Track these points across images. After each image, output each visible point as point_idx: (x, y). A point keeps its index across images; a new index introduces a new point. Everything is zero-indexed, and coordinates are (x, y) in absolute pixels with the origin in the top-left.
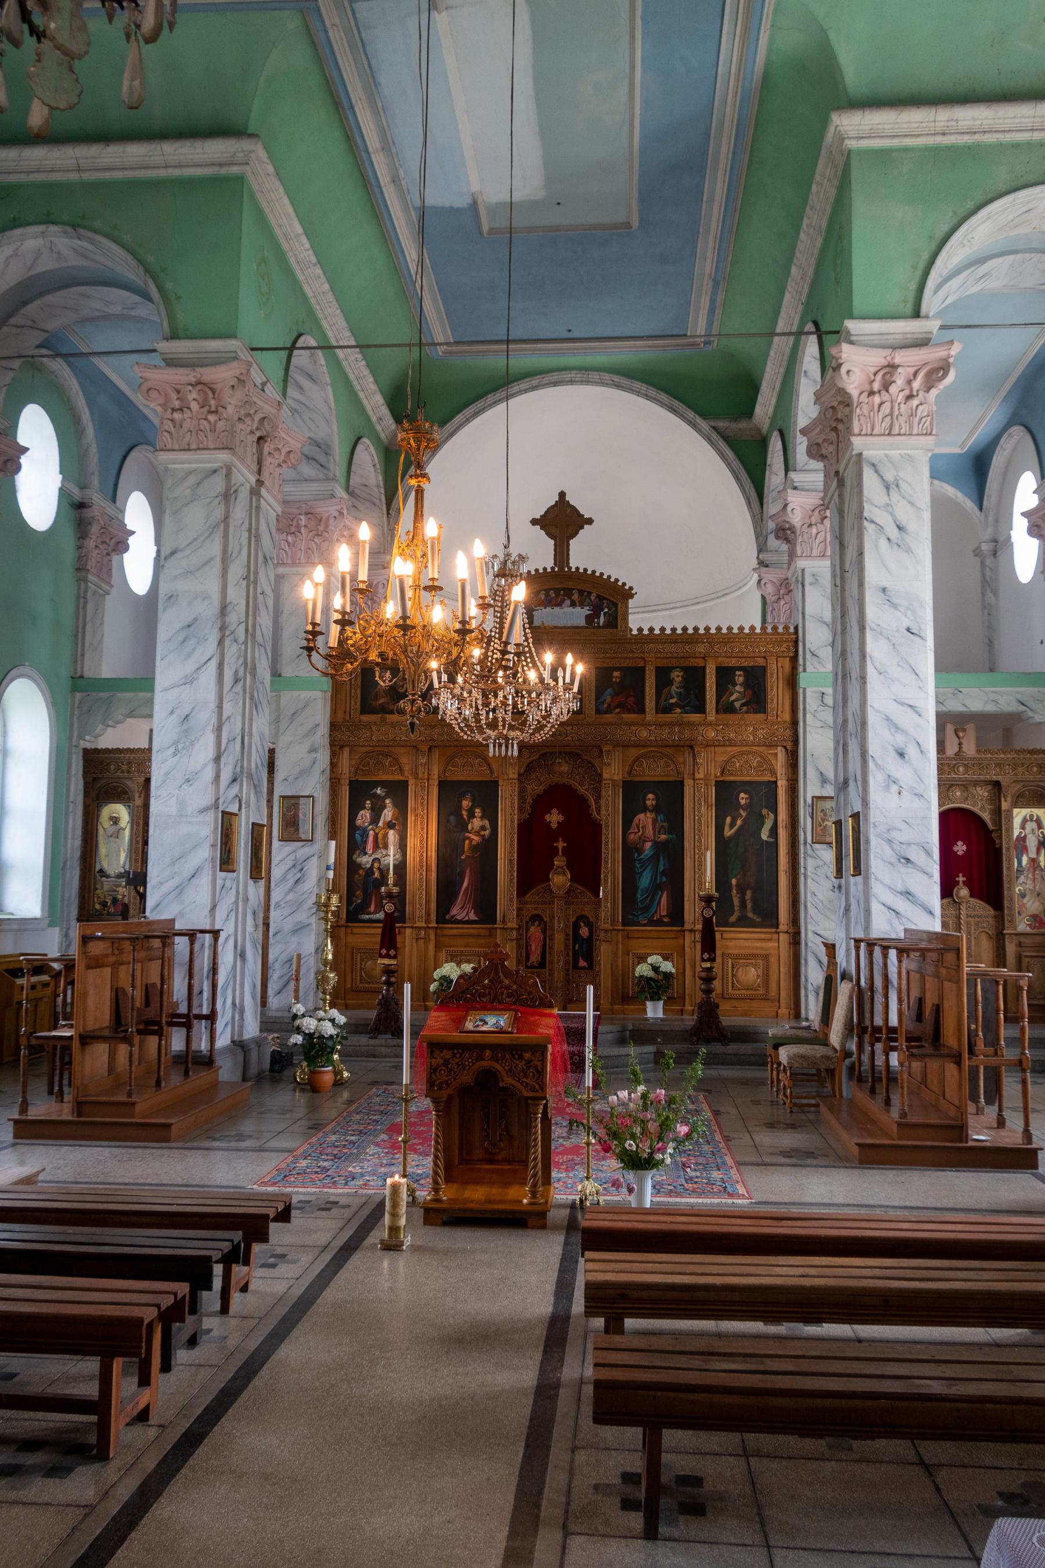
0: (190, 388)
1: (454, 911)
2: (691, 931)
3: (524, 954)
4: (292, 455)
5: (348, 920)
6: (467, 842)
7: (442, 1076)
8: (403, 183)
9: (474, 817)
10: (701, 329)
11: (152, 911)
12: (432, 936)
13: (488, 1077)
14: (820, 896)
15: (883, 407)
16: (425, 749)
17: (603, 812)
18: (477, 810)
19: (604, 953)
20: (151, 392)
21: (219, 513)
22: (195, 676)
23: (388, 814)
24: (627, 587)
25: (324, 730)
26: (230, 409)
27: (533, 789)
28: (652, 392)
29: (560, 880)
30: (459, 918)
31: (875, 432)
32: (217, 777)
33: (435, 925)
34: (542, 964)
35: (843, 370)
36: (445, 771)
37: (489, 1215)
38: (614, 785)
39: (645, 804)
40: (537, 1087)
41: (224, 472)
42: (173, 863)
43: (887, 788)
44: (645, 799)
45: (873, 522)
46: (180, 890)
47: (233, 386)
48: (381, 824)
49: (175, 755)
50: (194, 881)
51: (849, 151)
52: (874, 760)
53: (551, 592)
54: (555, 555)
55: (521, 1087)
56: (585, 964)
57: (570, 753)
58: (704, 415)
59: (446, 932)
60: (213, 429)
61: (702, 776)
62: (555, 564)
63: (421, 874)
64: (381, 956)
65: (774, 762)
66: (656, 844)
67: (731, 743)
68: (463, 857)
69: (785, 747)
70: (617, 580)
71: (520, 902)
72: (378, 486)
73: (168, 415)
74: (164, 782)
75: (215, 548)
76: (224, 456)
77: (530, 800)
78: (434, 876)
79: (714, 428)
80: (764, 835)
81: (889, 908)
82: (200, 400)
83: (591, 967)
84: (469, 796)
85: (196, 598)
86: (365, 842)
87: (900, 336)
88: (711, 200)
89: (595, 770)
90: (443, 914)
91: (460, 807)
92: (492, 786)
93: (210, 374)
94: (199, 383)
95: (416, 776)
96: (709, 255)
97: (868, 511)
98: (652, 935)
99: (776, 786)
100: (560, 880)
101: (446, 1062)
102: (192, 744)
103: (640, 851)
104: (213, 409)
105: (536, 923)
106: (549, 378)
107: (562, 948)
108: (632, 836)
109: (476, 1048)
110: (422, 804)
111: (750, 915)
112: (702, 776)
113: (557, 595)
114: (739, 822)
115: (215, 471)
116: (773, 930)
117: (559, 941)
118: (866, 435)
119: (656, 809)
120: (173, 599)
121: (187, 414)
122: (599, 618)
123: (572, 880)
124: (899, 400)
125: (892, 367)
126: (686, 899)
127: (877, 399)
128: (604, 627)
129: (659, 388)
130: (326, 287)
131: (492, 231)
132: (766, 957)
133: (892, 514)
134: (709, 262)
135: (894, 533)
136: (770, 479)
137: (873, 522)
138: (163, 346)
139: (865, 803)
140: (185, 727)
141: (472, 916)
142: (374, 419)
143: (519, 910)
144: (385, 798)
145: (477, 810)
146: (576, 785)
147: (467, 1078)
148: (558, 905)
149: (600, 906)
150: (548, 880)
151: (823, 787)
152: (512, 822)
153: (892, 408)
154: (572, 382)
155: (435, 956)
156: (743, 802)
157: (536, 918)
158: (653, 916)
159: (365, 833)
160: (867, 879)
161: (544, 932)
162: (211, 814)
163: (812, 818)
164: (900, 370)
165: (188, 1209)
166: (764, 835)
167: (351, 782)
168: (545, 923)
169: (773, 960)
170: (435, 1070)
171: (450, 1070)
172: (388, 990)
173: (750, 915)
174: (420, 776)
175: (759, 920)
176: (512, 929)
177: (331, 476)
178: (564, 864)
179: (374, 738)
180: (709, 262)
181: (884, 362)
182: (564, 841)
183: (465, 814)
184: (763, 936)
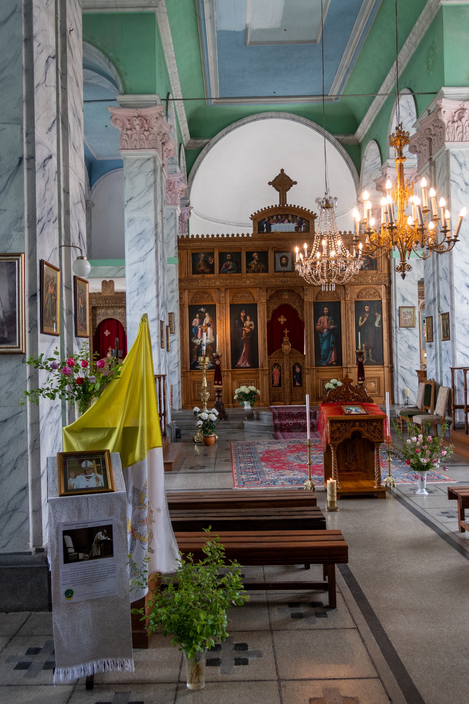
0: (135, 118)
1: (239, 363)
2: (346, 368)
3: (271, 381)
4: (171, 152)
5: (191, 369)
6: (244, 332)
7: (337, 435)
8: (215, 18)
9: (247, 320)
10: (335, 93)
12: (230, 375)
13: (357, 435)
14: (403, 350)
15: (459, 128)
16: (223, 290)
17: (305, 316)
18: (248, 317)
19: (307, 379)
20: (117, 120)
21: (152, 180)
22: (145, 257)
23: (207, 320)
24: (313, 214)
25: (176, 282)
26: (155, 129)
27: (273, 307)
28: (309, 122)
29: (286, 347)
30: (242, 366)
31: (450, 140)
32: (158, 305)
33: (231, 369)
34: (280, 385)
35: (442, 111)
36: (232, 300)
37: (360, 494)
38: (309, 304)
39: (323, 312)
40: (379, 437)
41: (152, 160)
43: (462, 301)
44: (323, 310)
45: (454, 182)
47: (157, 118)
48: (204, 325)
49: (137, 295)
51: (442, 6)
52: (456, 289)
53: (279, 216)
54: (280, 199)
55: (372, 438)
56: (299, 384)
57: (289, 290)
58: (333, 133)
59: (236, 372)
60: (147, 139)
61: (349, 299)
62: (280, 203)
63: (224, 347)
64: (215, 384)
65: (380, 292)
66: (329, 330)
67: (361, 284)
68: (242, 339)
69: (385, 285)
70: (309, 210)
71: (269, 358)
72: (184, 167)
73: (125, 131)
75: (151, 196)
76: (153, 152)
77: (271, 311)
78: (229, 347)
79: (337, 139)
80: (377, 325)
81: (464, 354)
82: (140, 125)
83: (301, 385)
84: (244, 311)
85: (143, 220)
86: (197, 333)
87: (466, 95)
88: (357, 30)
89: (301, 298)
90: (234, 365)
91: (240, 316)
92: (254, 306)
93: (144, 112)
94: (139, 116)
95: (220, 302)
96: (348, 56)
97: (452, 177)
98: (329, 370)
99: (382, 303)
100: (286, 347)
101: (338, 429)
102: (145, 289)
103: (322, 333)
104: (146, 129)
105: (276, 367)
106: (261, 115)
107: (288, 377)
108: (318, 327)
109: (352, 421)
110: (223, 315)
111: (371, 360)
112: (349, 299)
113: (282, 218)
114: (365, 319)
115: (149, 159)
116: (340, 367)
117: (287, 375)
118: (451, 141)
119: (329, 314)
120: (132, 221)
121: (134, 131)
122: (301, 228)
123: (292, 347)
124: (466, 125)
125: (463, 110)
126: (343, 353)
127: (456, 125)
128: (304, 232)
129: (312, 120)
130: (176, 70)
131: (251, 43)
132: (379, 378)
133: (463, 178)
134: (347, 60)
135: (464, 187)
136: (364, 163)
137: (454, 182)
138: (121, 98)
139: (452, 308)
140: (142, 281)
141: (248, 365)
142: (183, 135)
143: (268, 361)
144: (205, 313)
145: (248, 317)
146: (292, 304)
147: (348, 435)
148: (286, 359)
149: (305, 358)
150: (281, 347)
151: (403, 302)
152: (264, 322)
153: (463, 129)
154: (272, 117)
155: (232, 383)
156: (367, 310)
157: (276, 365)
158: (328, 362)
159: (197, 329)
160: (453, 342)
161: (280, 371)
162: (156, 321)
163: (399, 316)
164: (467, 111)
165: (277, 498)
166: (377, 325)
167: (189, 306)
168: (280, 367)
169: (382, 379)
170: (334, 432)
171: (340, 432)
172: (218, 399)
173: (371, 360)
174: (221, 302)
175: (375, 362)
176: (266, 370)
177: (175, 162)
178: (288, 340)
179: (199, 285)
180: (347, 60)
181: (459, 107)
182: (288, 330)
183: (242, 319)
184: (377, 369)
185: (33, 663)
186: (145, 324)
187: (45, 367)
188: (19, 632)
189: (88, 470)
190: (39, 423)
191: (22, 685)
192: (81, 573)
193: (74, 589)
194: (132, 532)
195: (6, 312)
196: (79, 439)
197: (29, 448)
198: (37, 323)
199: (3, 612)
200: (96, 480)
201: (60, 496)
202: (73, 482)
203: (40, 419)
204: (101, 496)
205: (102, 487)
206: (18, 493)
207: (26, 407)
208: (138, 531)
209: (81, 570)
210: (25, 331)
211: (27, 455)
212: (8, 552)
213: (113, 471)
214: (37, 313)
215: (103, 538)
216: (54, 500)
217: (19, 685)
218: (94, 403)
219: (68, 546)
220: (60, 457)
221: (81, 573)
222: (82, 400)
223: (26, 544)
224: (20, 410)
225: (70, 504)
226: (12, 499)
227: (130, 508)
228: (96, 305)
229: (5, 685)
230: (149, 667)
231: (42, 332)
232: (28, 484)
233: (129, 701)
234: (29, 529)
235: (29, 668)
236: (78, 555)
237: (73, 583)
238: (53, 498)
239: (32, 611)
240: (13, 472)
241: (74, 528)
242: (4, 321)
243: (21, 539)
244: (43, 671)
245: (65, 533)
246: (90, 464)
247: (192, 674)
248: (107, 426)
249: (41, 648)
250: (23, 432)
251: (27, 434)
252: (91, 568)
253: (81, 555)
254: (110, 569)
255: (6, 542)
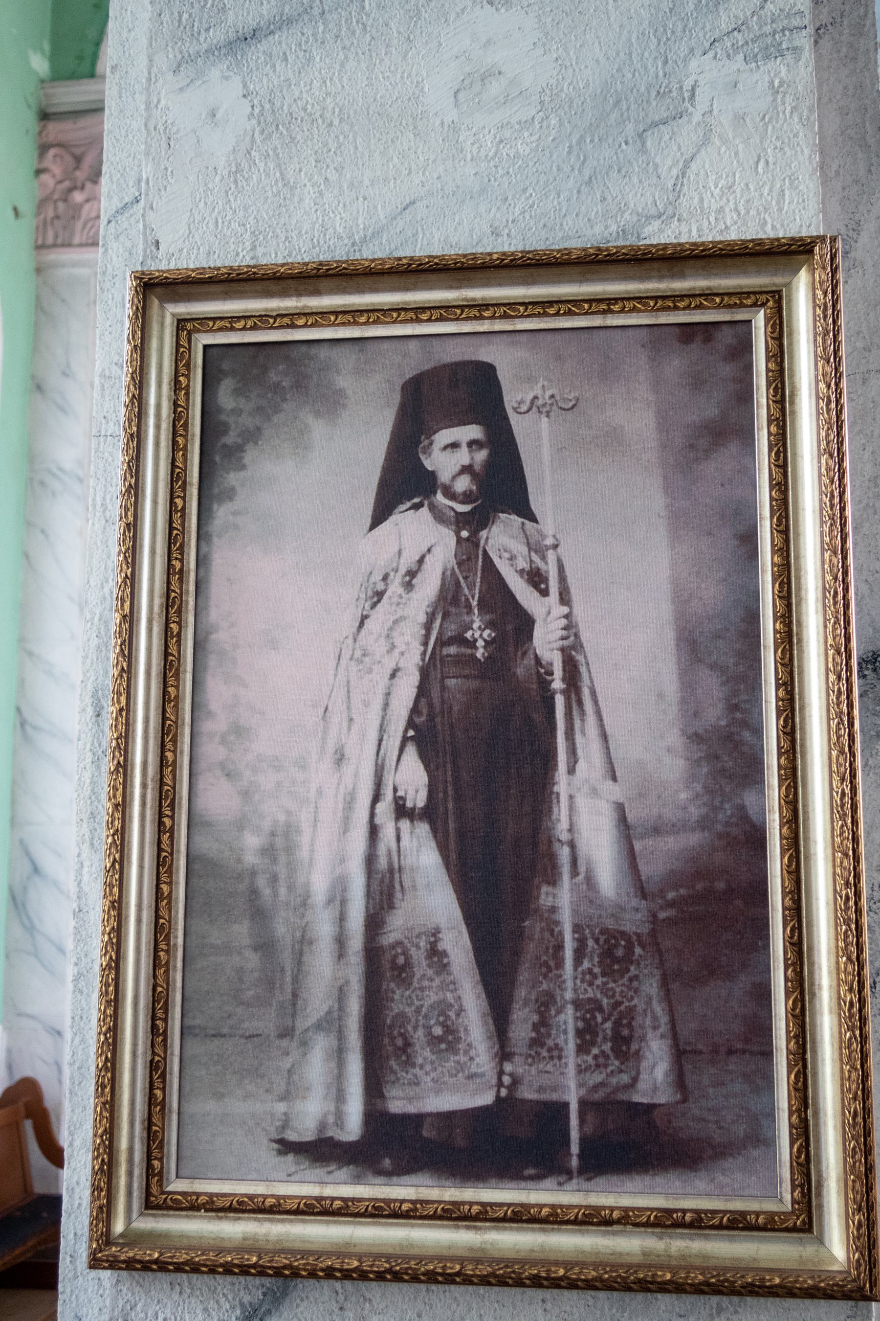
195: (656, 830)
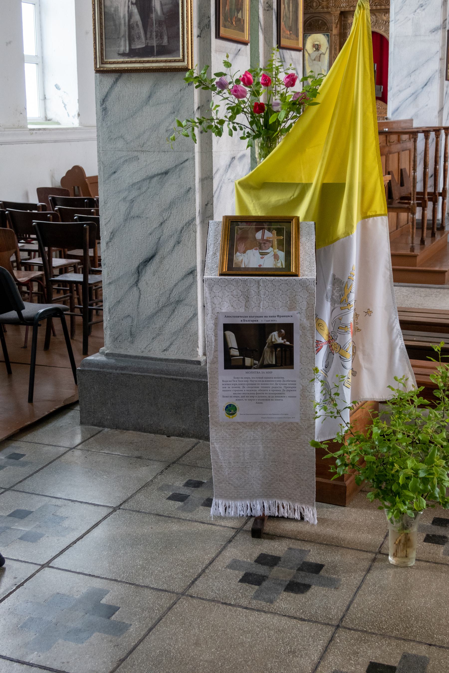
11: (393, 114)
42: (409, 75)
46: (415, 95)
50: (427, 88)
74: (401, 8)
185: (191, 497)
186: (363, 13)
187: (210, 86)
188: (180, 460)
189: (264, 243)
190: (212, 179)
191: (174, 518)
192: (248, 384)
193: (237, 404)
194: (329, 342)
195: (165, 5)
196: (258, 198)
197: (197, 214)
198: (210, 21)
199: (163, 434)
200: (275, 258)
201: (221, 275)
202: (240, 258)
203: (214, 172)
204: (278, 281)
205: (282, 268)
206: (183, 279)
207: (194, 153)
208: (337, 341)
209: (247, 381)
210: (191, 34)
211: (195, 225)
212: (170, 358)
213: (301, 248)
214: (209, 5)
215: (280, 341)
216: (211, 279)
217: (169, 517)
218: (280, 144)
219: (230, 346)
220: (226, 222)
221: (248, 384)
222: (263, 139)
223: (193, 350)
224: (186, 158)
225: (233, 288)
226: (175, 285)
227: (327, 307)
228: (347, 9)
229: (154, 514)
230: (342, 529)
231: (218, 36)
232: (196, 266)
233: (305, 560)
234: (198, 330)
235: (186, 501)
236: (244, 360)
237: (237, 397)
238: (210, 277)
239: (200, 438)
240: (176, 248)
241: (238, 321)
242: (163, 19)
243: (187, 343)
244: (201, 508)
245: (227, 327)
246: (268, 235)
247: (398, 545)
248: (297, 181)
249: (204, 483)
250: (190, 190)
251: (194, 194)
252: (261, 380)
253: (248, 361)
254: (287, 386)
255: (168, 344)
